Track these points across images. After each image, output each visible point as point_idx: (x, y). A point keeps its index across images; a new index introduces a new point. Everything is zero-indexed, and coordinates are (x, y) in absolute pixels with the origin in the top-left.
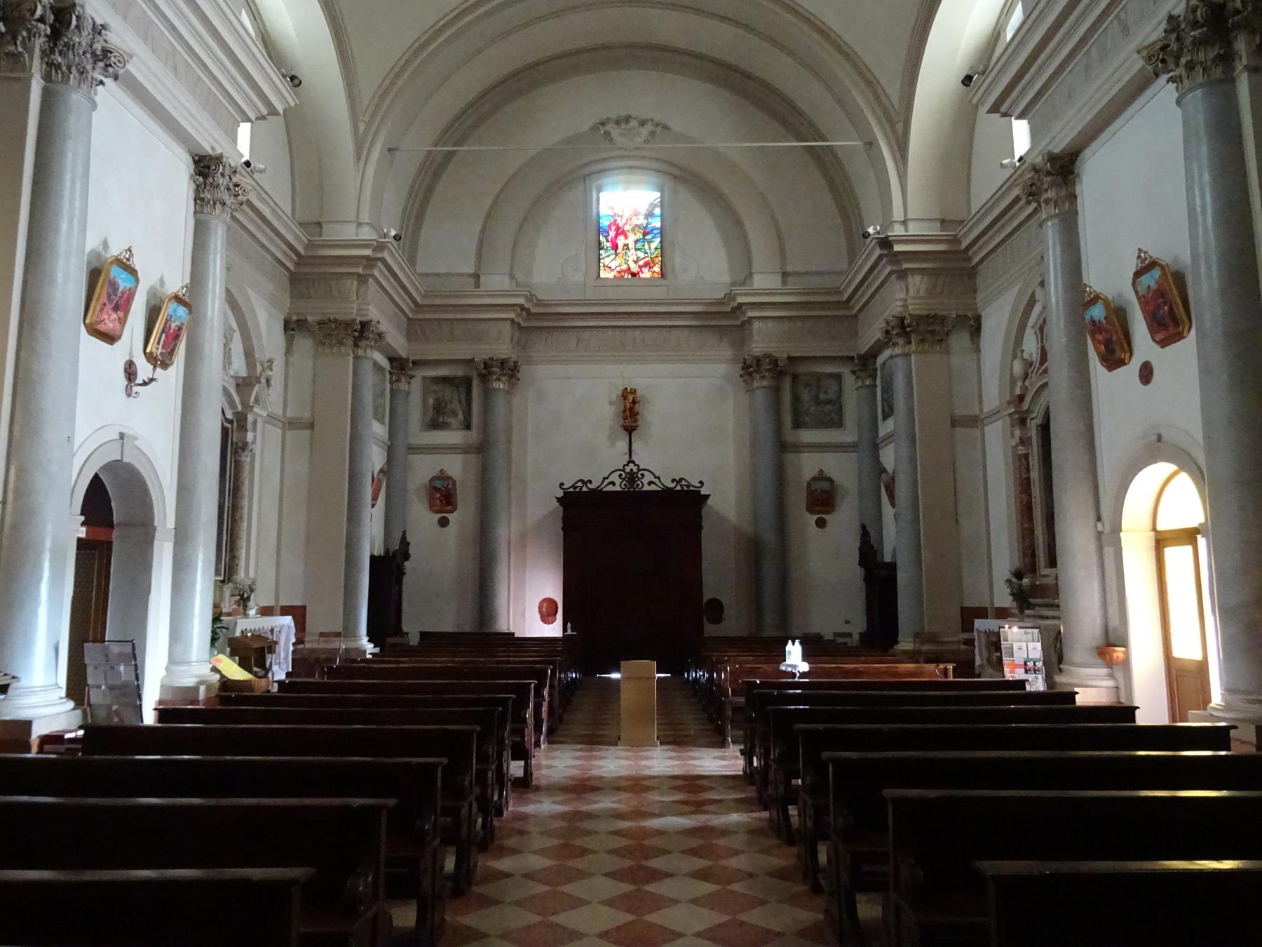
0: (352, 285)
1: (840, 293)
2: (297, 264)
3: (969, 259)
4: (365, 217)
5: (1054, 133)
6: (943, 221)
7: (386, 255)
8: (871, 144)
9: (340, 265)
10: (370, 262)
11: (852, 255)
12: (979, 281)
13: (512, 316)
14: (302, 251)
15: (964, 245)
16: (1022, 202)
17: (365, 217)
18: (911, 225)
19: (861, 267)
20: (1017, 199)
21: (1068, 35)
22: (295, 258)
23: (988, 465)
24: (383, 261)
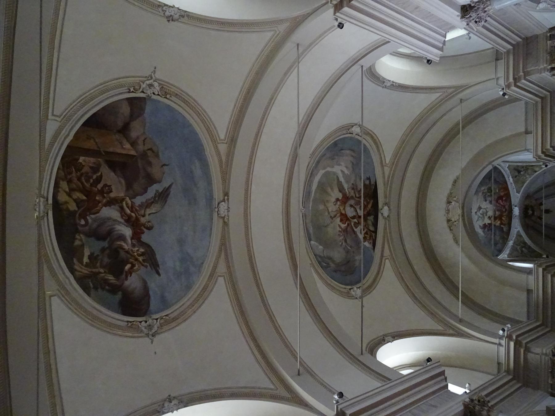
0: (530, 356)
1: (537, 102)
2: (518, 382)
3: (518, 43)
4: (497, 341)
5: (523, 18)
6: (497, 59)
7: (524, 342)
8: (461, 100)
9: (519, 358)
10: (517, 344)
11: (517, 100)
12: (530, 35)
13: (549, 276)
14: (511, 377)
15: (510, 47)
16: (486, 24)
17: (497, 341)
18: (499, 75)
19: (517, 93)
20: (484, 27)
21: (414, 28)
22: (514, 382)
23: (16, 35)
24: (527, 343)
